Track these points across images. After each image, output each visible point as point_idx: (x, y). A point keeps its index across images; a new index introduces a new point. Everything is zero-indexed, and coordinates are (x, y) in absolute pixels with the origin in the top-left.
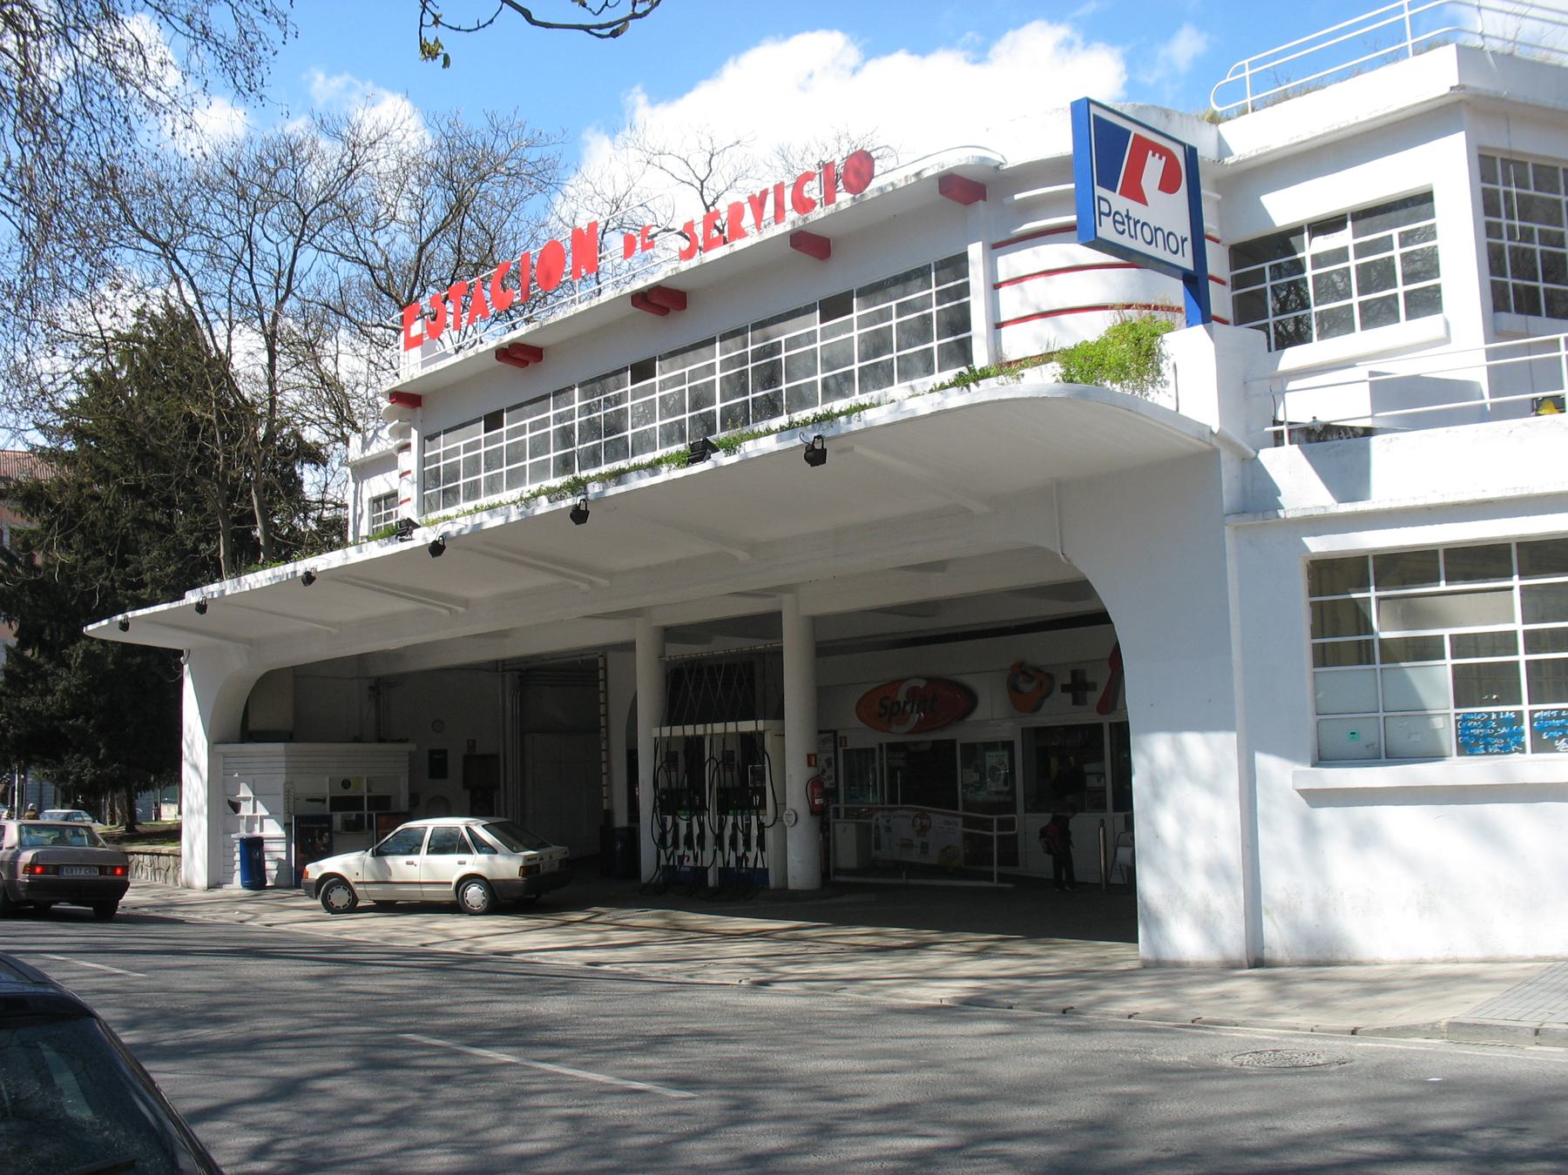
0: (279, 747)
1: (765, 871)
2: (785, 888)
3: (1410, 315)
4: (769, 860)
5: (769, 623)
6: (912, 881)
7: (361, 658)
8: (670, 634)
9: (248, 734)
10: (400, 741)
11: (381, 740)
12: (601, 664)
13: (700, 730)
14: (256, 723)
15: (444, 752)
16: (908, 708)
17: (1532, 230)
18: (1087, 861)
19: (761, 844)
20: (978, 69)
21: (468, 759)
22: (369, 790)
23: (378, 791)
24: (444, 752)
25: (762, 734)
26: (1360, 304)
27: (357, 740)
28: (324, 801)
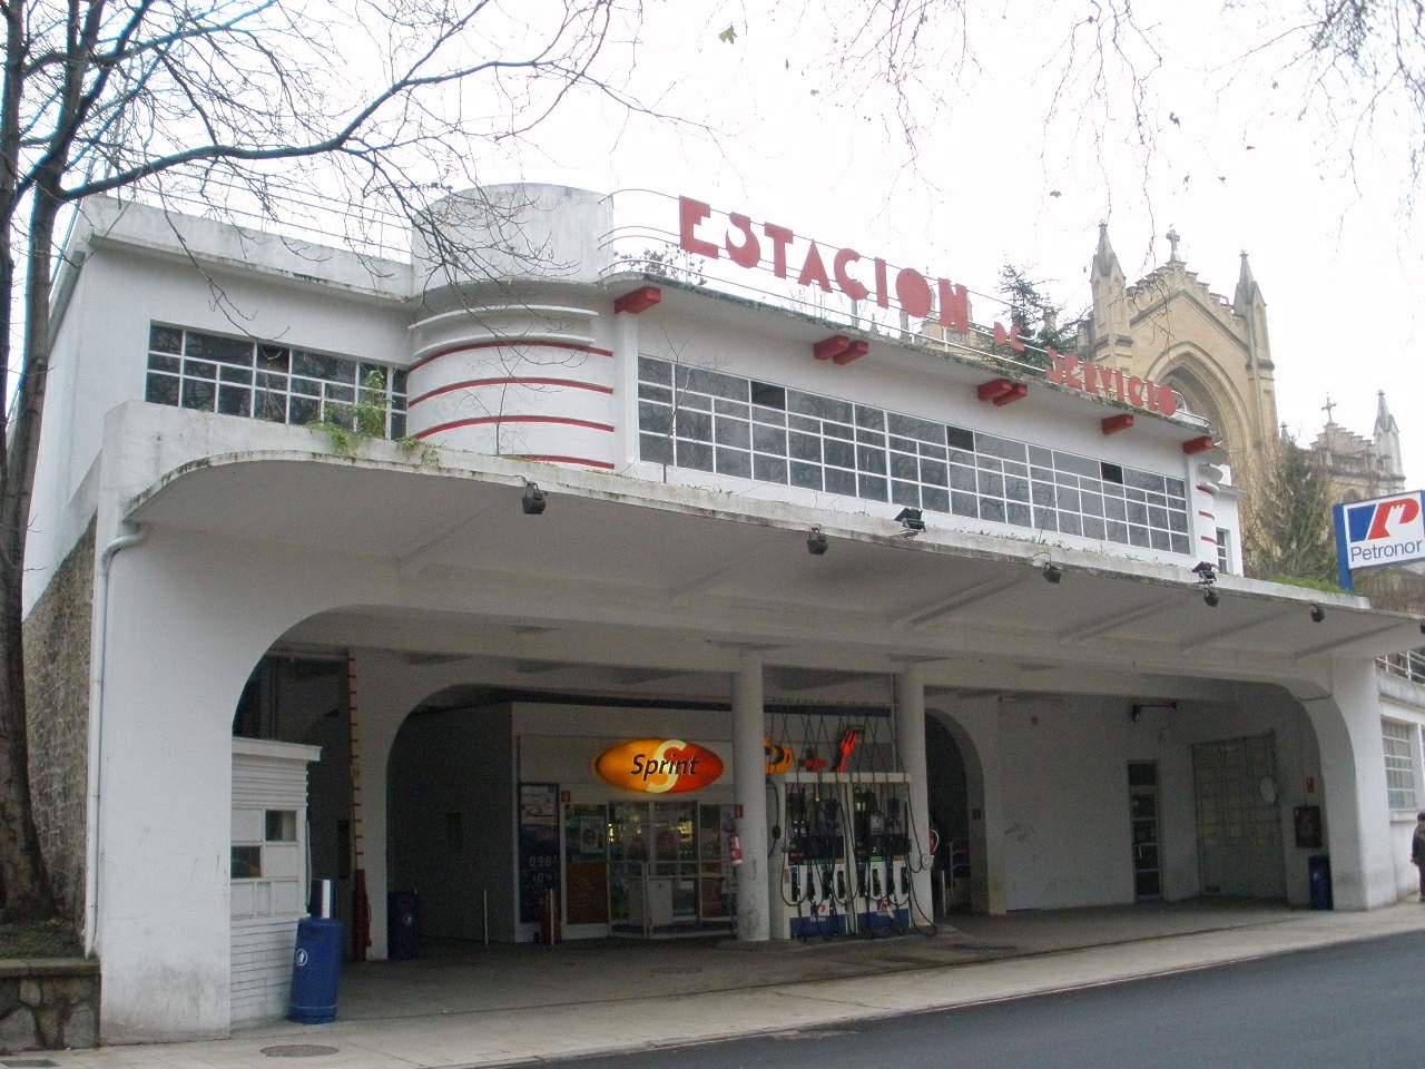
16: (666, 768)
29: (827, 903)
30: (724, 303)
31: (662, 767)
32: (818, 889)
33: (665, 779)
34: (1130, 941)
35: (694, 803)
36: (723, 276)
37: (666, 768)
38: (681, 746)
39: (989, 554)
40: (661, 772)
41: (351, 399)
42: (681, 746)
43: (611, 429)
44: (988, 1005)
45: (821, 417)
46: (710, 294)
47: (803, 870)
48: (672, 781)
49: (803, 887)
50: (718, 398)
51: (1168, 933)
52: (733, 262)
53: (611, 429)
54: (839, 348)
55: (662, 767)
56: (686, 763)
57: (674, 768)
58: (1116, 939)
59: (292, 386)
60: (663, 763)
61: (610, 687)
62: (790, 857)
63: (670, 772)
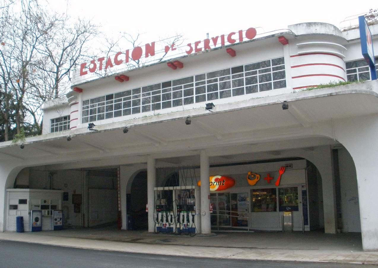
0: (28, 190)
1: (195, 228)
2: (200, 233)
3: (174, 106)
4: (196, 225)
5: (198, 157)
6: (220, 231)
7: (46, 166)
8: (157, 160)
9: (16, 186)
10: (59, 189)
11: (50, 189)
12: (118, 169)
13: (171, 188)
14: (19, 183)
15: (67, 193)
16: (215, 184)
17: (368, 70)
18: (349, 228)
19: (193, 221)
20: (146, 43)
21: (73, 195)
22: (51, 204)
23: (54, 204)
24: (67, 193)
25: (194, 190)
26: (162, 103)
27: (44, 189)
28: (39, 206)
29: (167, 224)
30: (86, 84)
31: (214, 184)
32: (165, 219)
33: (214, 187)
34: (223, 247)
35: (229, 194)
36: (90, 77)
37: (215, 184)
38: (219, 177)
39: (57, 138)
40: (214, 185)
41: (359, 69)
42: (219, 177)
43: (293, 78)
44: (87, 249)
45: (182, 84)
46: (147, 66)
47: (160, 214)
48: (217, 187)
49: (160, 218)
50: (98, 103)
51: (248, 247)
52: (254, 28)
53: (293, 78)
54: (122, 78)
55: (214, 184)
56: (221, 182)
57: (218, 183)
58: (208, 245)
59: (99, 115)
60: (214, 182)
61: (225, 161)
62: (157, 210)
63: (216, 185)
